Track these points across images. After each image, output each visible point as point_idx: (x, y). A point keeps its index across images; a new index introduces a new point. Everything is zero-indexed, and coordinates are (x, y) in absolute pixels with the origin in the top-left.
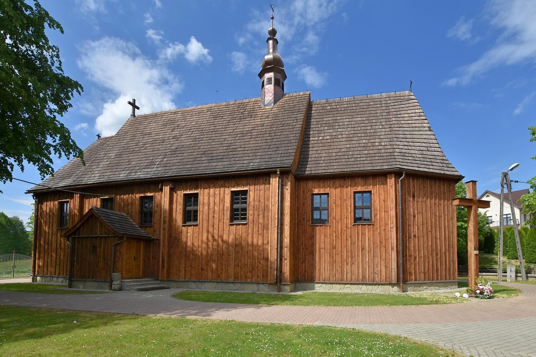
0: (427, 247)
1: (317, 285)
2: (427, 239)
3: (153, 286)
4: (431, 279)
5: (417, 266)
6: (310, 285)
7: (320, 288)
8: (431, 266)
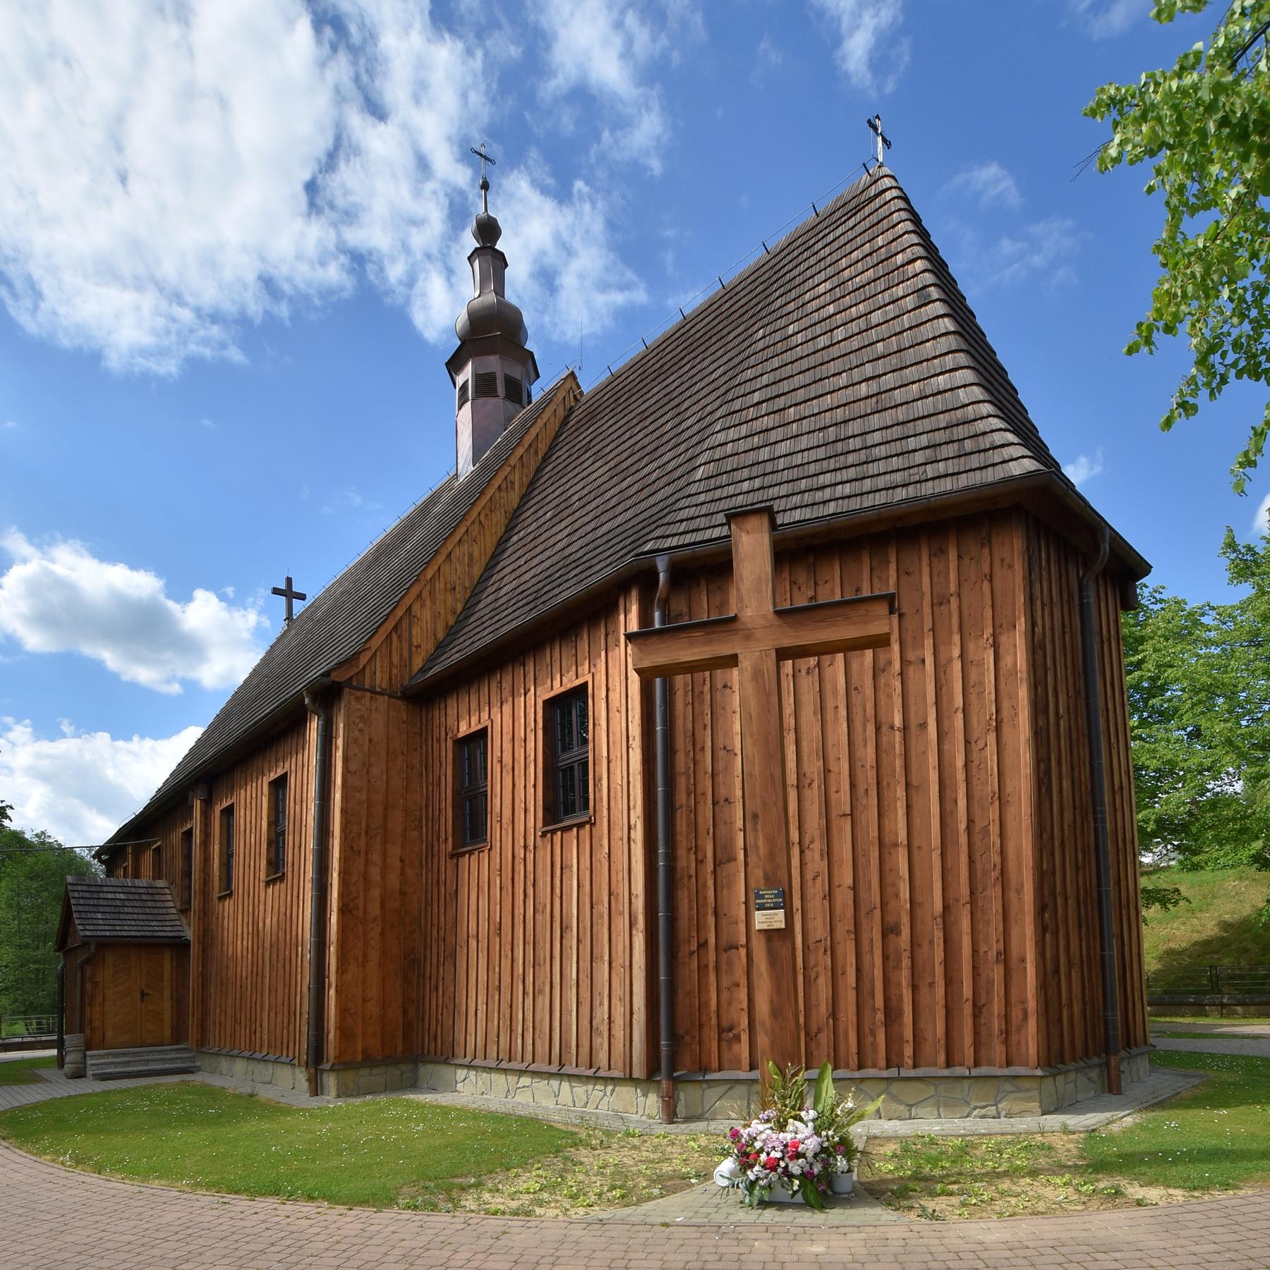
0: (830, 896)
1: (461, 1073)
2: (829, 853)
3: (167, 1066)
4: (854, 1061)
5: (745, 996)
6: (445, 1070)
7: (471, 1091)
8: (851, 996)
